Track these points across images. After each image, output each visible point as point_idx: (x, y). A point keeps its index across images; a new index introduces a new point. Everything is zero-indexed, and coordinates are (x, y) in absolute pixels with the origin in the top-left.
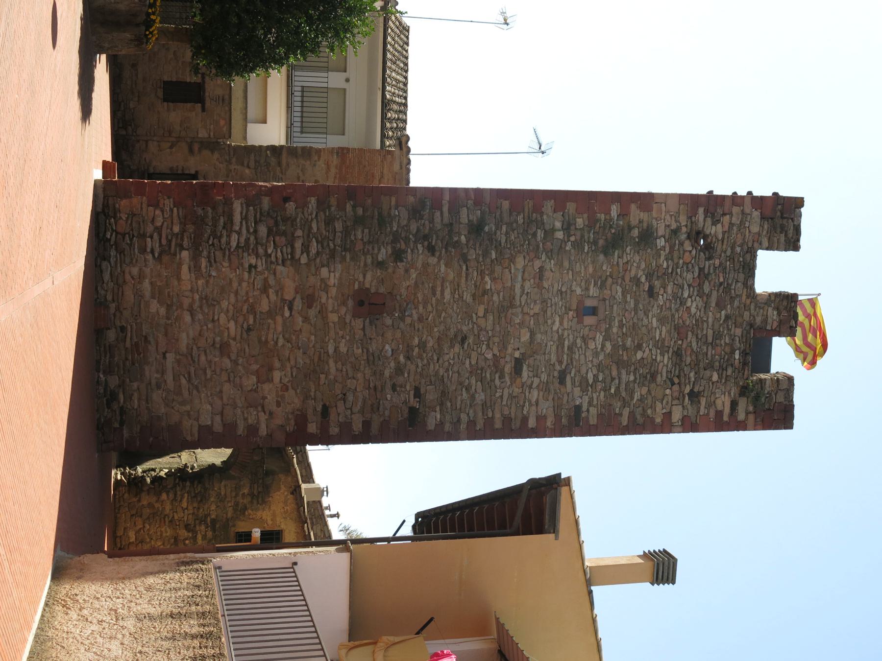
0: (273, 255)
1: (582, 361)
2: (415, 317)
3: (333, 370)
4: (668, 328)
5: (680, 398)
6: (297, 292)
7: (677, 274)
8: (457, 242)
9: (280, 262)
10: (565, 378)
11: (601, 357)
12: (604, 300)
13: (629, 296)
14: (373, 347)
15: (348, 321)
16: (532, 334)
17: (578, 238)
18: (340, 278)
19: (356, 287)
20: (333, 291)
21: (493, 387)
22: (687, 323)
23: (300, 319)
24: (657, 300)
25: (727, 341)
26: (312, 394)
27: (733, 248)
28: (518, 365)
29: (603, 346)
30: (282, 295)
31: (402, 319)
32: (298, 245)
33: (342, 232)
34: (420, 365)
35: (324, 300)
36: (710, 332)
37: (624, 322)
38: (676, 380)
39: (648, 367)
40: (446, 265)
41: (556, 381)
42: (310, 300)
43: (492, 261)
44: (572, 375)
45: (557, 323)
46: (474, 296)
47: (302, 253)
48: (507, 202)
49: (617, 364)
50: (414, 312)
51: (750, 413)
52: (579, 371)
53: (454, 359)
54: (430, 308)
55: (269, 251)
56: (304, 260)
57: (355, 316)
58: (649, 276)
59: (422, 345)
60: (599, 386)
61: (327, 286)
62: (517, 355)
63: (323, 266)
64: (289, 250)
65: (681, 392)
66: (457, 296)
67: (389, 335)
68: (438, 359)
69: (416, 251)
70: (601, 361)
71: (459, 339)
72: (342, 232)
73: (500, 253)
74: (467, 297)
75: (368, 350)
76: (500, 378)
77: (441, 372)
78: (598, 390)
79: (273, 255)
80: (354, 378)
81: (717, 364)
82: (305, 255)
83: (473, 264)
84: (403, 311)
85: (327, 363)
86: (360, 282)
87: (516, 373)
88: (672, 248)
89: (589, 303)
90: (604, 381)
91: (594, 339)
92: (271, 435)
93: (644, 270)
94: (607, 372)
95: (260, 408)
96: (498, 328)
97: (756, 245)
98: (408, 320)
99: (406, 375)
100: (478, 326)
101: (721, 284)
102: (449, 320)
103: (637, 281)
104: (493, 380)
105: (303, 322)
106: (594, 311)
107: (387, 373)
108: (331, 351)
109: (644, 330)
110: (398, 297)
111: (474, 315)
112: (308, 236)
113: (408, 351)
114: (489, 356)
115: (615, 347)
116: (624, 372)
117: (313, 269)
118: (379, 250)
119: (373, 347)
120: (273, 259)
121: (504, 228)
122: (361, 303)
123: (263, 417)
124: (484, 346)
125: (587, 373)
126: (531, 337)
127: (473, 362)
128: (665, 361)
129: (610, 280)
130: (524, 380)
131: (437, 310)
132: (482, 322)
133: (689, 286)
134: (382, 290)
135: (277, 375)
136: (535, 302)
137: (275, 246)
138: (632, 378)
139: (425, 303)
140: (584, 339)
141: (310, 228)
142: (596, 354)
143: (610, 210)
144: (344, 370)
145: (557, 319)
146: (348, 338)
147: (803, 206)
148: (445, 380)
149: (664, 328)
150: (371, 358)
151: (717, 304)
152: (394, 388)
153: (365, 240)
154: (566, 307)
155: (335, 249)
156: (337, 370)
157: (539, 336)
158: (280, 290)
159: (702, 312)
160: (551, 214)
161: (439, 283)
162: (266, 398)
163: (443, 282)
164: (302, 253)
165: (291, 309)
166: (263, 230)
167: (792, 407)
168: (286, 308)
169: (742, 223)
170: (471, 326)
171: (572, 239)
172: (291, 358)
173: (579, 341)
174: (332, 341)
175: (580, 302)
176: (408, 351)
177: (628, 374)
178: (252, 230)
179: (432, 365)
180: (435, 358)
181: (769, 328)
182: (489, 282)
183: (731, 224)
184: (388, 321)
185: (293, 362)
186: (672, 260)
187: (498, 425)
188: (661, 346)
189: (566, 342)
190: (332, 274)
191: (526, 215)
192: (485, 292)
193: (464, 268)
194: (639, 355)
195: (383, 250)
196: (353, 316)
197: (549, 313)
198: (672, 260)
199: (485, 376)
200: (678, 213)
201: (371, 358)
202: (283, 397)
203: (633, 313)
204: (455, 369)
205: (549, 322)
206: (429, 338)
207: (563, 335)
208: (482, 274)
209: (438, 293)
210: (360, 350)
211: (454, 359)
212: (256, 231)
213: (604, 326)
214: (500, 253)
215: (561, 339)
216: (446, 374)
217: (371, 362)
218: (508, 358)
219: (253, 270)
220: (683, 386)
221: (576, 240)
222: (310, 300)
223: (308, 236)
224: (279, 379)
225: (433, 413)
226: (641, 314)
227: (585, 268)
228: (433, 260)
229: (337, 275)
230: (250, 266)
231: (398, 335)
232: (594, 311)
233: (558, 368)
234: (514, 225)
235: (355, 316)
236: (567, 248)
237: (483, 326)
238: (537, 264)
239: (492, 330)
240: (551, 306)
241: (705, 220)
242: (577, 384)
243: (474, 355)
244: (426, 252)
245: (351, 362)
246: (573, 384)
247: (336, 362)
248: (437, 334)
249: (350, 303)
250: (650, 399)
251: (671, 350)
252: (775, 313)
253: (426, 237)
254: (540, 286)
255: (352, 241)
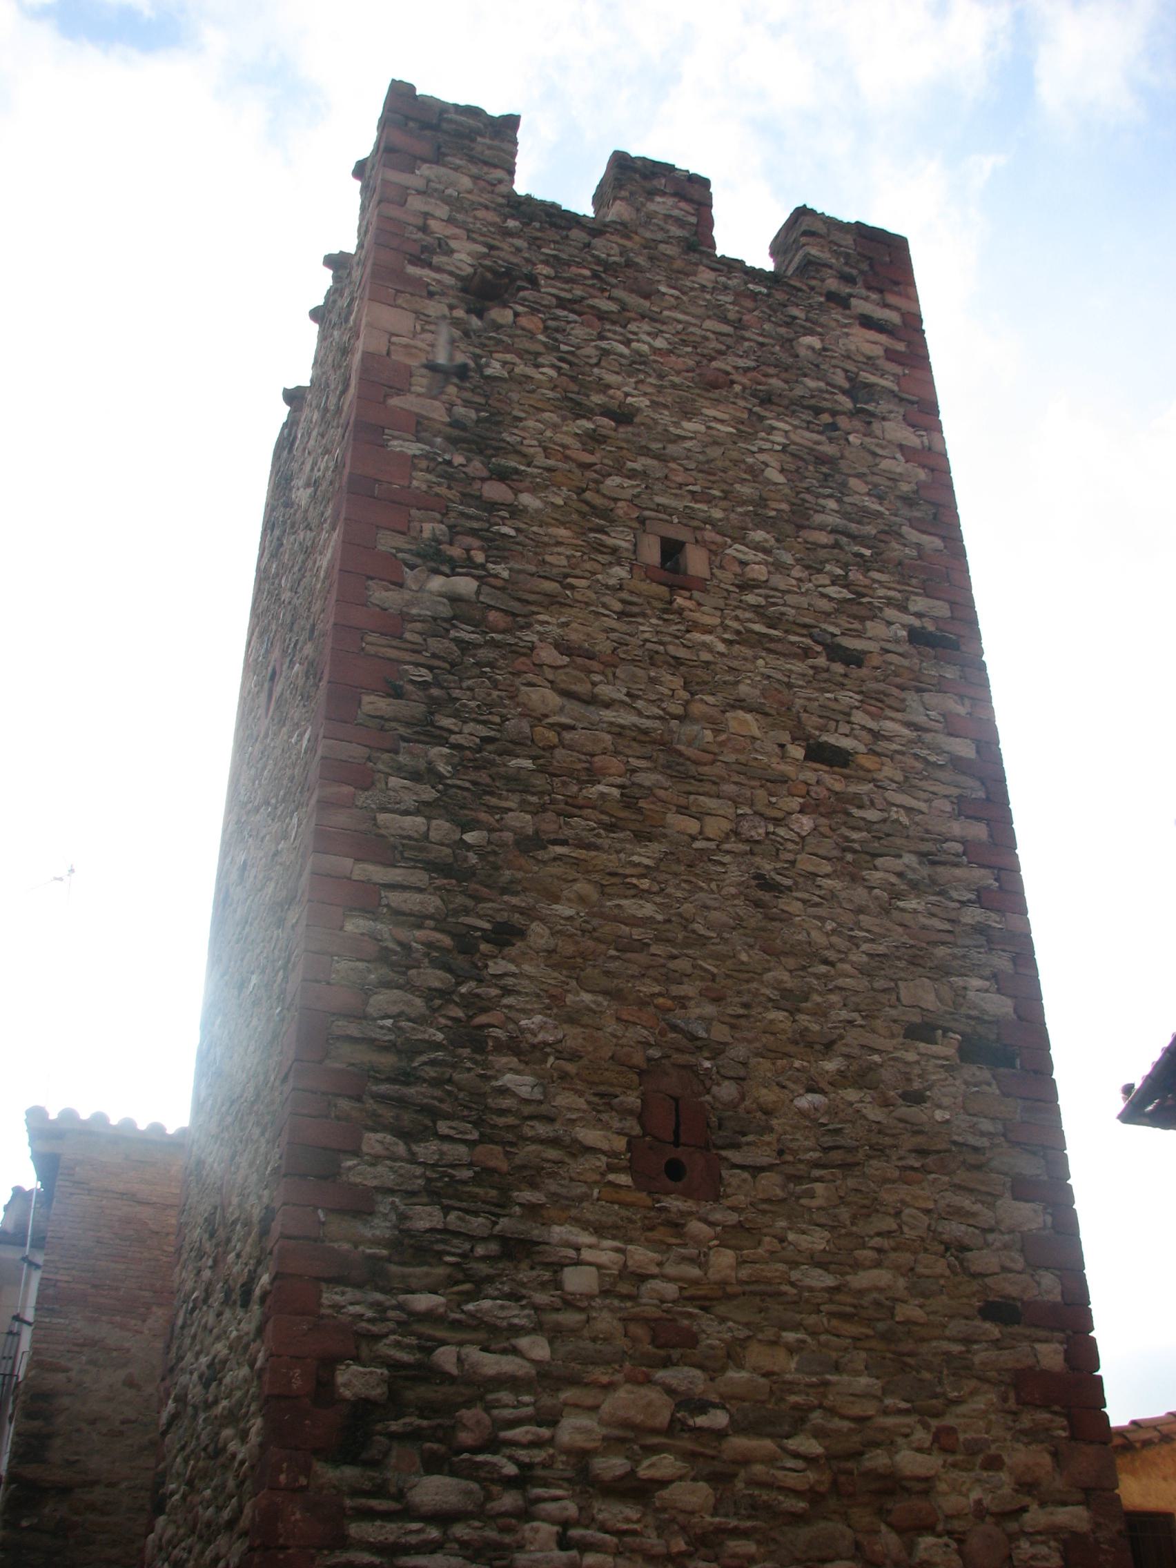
0: (523, 1455)
1: (804, 602)
2: (709, 1010)
3: (882, 1277)
4: (707, 403)
5: (868, 418)
6: (648, 1381)
7: (572, 353)
8: (482, 856)
9: (545, 1432)
10: (839, 646)
11: (788, 558)
12: (642, 521)
13: (630, 465)
14: (806, 1145)
15: (733, 1218)
16: (739, 704)
17: (476, 543)
18: (599, 1230)
19: (624, 1179)
20: (641, 1255)
21: (886, 828)
22: (691, 363)
23: (732, 1374)
24: (638, 410)
25: (730, 299)
26: (956, 1348)
27: (507, 233)
28: (820, 754)
29: (757, 547)
30: (655, 1431)
31: (717, 1051)
32: (492, 1364)
33: (446, 1210)
34: (844, 1014)
35: (671, 1290)
36: (708, 324)
37: (696, 488)
38: (826, 418)
39: (801, 464)
40: (556, 899)
41: (854, 671)
42: (668, 1340)
43: (541, 770)
44: (837, 631)
45: (708, 638)
46: (642, 837)
47: (515, 1351)
48: (366, 699)
49: (800, 527)
50: (695, 1012)
51: (883, 299)
52: (828, 614)
53: (822, 919)
54: (683, 965)
55: (511, 1469)
56: (538, 1348)
57: (713, 1191)
58: (580, 411)
59: (791, 1001)
60: (855, 575)
61: (625, 1273)
62: (798, 752)
63: (558, 1284)
64: (505, 1396)
65: (852, 414)
66: (645, 884)
67: (768, 1096)
68: (826, 962)
69: (510, 981)
70: (797, 560)
71: (766, 897)
72: (446, 1210)
73: (516, 745)
74: (644, 855)
75: (816, 1165)
76: (860, 807)
77: (857, 957)
78: (867, 582)
79: (523, 1455)
80: (898, 1214)
81: (782, 330)
82: (523, 1342)
83: (549, 824)
84: (696, 1044)
85: (861, 1293)
86: (611, 1169)
87: (845, 765)
88: (508, 349)
89: (652, 553)
90: (845, 566)
91: (744, 564)
92: (1086, 1490)
93: (564, 419)
94: (822, 554)
95: (1013, 1526)
96: (728, 788)
97: (502, 189)
98: (720, 1033)
99: (876, 1058)
100: (727, 837)
101: (595, 276)
102: (714, 915)
103: (594, 439)
104: (868, 825)
105: (741, 1367)
106: (672, 550)
107: (874, 1113)
108: (821, 1279)
109: (714, 452)
110: (655, 1053)
111: (698, 845)
112: (456, 1325)
113: (810, 1045)
114: (806, 823)
115: (763, 522)
116: (818, 518)
117: (570, 1318)
118: (504, 1091)
119: (806, 1145)
120: (539, 1455)
121: (447, 722)
122: (675, 1170)
123: (1036, 1517)
124: (782, 831)
125: (831, 599)
126: (750, 710)
127: (828, 869)
128: (784, 429)
129: (588, 495)
130: (862, 748)
131: (686, 944)
132: (715, 827)
133: (601, 337)
134: (632, 1100)
135: (910, 1462)
136: (653, 681)
137: (493, 1445)
138: (832, 504)
139: (670, 978)
140: (746, 586)
141: (429, 1316)
142: (779, 567)
143: (402, 455)
144: (876, 1242)
145: (697, 636)
146: (782, 1223)
147: (412, 88)
148: (881, 949)
149: (705, 411)
150: (836, 1156)
151: (647, 297)
152: (916, 1098)
153: (475, 1135)
154: (665, 611)
155: (502, 1239)
156: (878, 1264)
157: (743, 689)
158: (630, 1436)
159: (664, 328)
160: (407, 595)
161: (607, 929)
162: (979, 1502)
163: (602, 916)
164: (515, 1351)
165: (702, 1407)
166: (434, 1490)
167: (859, 225)
168: (701, 1421)
169: (447, 201)
170: (727, 859)
171: (479, 557)
172: (856, 1411)
173: (751, 598)
174: (795, 1275)
175: (649, 574)
176: (810, 1045)
177: (823, 510)
178: (434, 1533)
179: (840, 982)
180: (823, 969)
181: (693, 220)
182: (601, 788)
183: (450, 221)
184: (727, 1091)
185: (869, 1408)
186: (538, 354)
187: (979, 831)
188: (750, 427)
189: (757, 627)
190: (586, 1255)
191: (407, 657)
192: (629, 800)
193: (560, 850)
194: (773, 475)
195: (508, 1079)
196: (717, 1198)
197: (682, 653)
198: (538, 354)
199: (861, 842)
200: (418, 313)
201: (836, 1156)
202: (973, 1449)
203: (673, 465)
204: (848, 918)
205: (706, 656)
206: (769, 976)
207: (738, 633)
208: (574, 806)
209: (637, 933)
210: (819, 1187)
211: (822, 919)
212: (443, 1518)
213: (709, 535)
214: (516, 745)
215: (744, 638)
216: (865, 947)
217: (850, 1159)
218: (810, 776)
219: (575, 1533)
220: (839, 408)
221: (481, 549)
222: (668, 1340)
223: (456, 1325)
224: (920, 1457)
225: (971, 994)
226: (672, 449)
227: (559, 544)
228: (539, 935)
229: (585, 1238)
230: (564, 1543)
231: (764, 1067)
232: (672, 550)
233: (822, 661)
234: (435, 692)
235: (713, 1191)
236: (505, 574)
237: (726, 826)
238: (548, 654)
239: (737, 805)
240: (661, 643)
241: (438, 270)
242: (857, 625)
243: (806, 863)
244: (512, 951)
245: (854, 1219)
246: (859, 635)
247: (857, 1266)
248: (757, 954)
249: (675, 1204)
250: (876, 479)
251: (757, 409)
252: (658, 199)
253: (465, 943)
254: (610, 665)
255: (476, 1180)
